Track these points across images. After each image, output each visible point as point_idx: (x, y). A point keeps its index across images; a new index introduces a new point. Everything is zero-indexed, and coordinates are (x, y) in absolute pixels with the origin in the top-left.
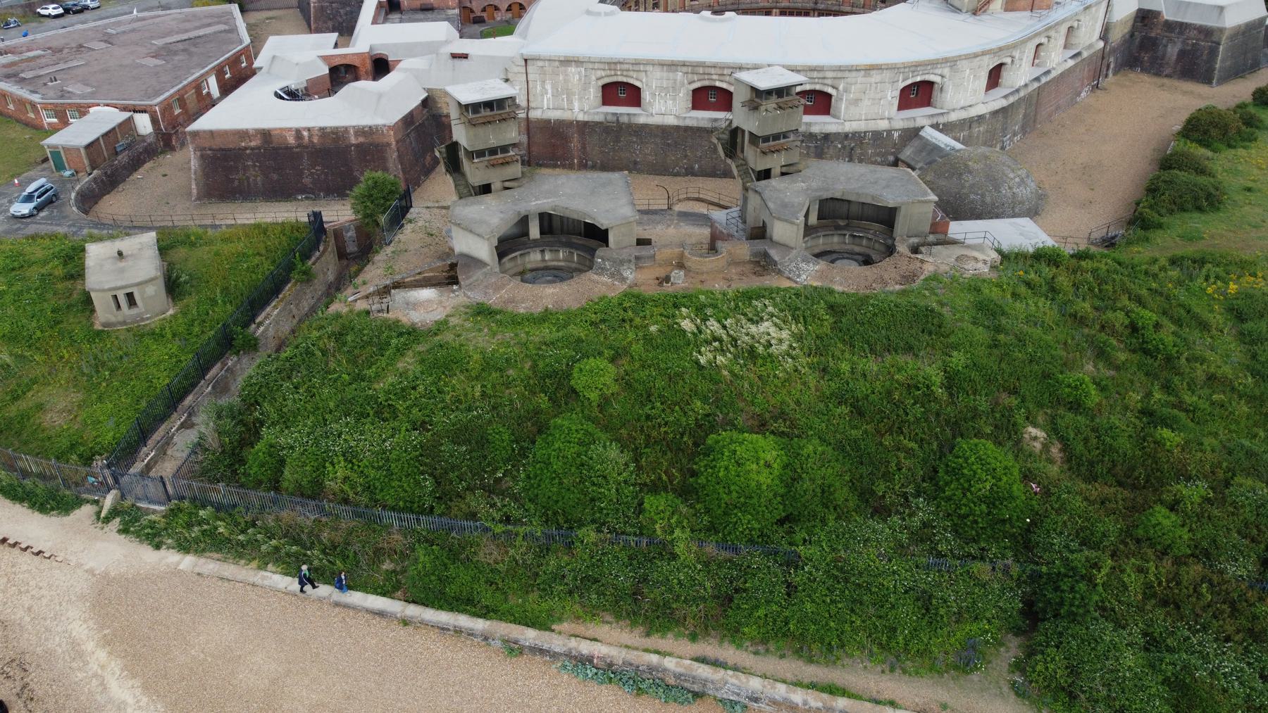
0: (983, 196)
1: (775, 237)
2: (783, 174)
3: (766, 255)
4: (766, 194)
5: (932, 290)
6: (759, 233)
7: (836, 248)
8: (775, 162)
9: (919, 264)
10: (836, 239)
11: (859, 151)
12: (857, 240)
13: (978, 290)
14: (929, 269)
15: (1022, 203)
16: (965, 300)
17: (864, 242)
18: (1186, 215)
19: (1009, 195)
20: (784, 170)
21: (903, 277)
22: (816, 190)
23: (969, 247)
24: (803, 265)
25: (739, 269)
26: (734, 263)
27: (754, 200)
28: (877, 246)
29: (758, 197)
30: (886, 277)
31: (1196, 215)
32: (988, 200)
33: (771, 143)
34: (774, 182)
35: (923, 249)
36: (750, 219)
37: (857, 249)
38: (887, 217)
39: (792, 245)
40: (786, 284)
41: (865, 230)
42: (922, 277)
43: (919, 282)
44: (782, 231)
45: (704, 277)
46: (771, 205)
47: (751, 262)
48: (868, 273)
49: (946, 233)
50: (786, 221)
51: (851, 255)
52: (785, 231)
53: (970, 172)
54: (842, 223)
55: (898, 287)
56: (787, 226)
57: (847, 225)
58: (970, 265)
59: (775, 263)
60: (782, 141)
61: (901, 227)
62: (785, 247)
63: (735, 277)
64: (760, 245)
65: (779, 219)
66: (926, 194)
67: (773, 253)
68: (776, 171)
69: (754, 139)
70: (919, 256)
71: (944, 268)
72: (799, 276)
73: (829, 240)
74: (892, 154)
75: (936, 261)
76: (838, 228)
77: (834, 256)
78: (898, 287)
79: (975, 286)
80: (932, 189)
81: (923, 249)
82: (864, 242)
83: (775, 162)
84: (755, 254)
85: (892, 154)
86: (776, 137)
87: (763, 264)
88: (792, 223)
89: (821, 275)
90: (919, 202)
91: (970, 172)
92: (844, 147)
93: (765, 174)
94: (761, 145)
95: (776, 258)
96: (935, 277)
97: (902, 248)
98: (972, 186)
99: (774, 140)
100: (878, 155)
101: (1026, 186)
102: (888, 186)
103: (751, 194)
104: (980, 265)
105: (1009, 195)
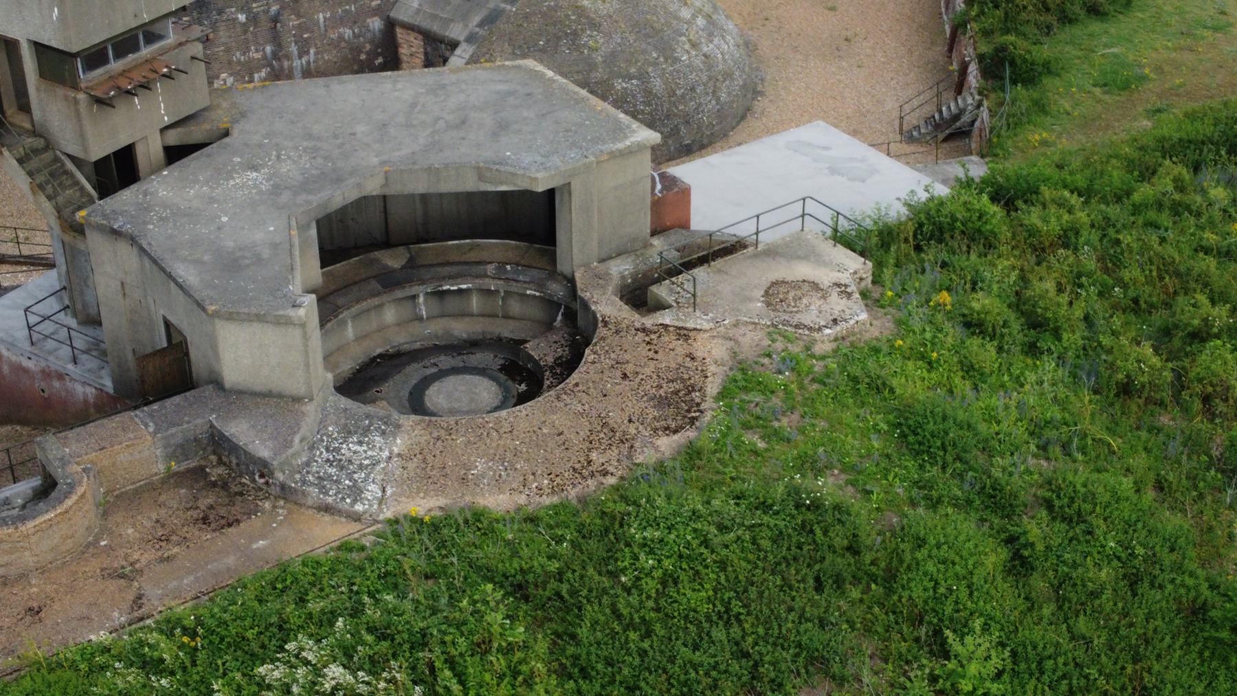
0: (643, 76)
1: (232, 374)
2: (174, 154)
3: (218, 443)
4: (155, 235)
5: (758, 423)
6: (165, 373)
7: (401, 339)
8: (142, 124)
9: (680, 347)
10: (390, 315)
11: (293, 22)
12: (452, 304)
13: (879, 387)
14: (713, 352)
15: (728, 75)
16: (862, 433)
17: (475, 303)
18: (1076, 30)
19: (698, 62)
20: (174, 138)
21: (662, 402)
22: (306, 186)
23: (772, 252)
24: (351, 448)
25: (147, 518)
26: (120, 500)
27: (111, 268)
28: (515, 307)
29: (124, 248)
30: (616, 418)
31: (1096, 26)
32: (657, 85)
33: (115, 66)
34: (162, 189)
35: (661, 291)
36: (114, 321)
37: (461, 329)
38: (530, 220)
39: (295, 386)
40: (323, 535)
41: (469, 268)
42: (712, 388)
43: (711, 410)
44: (242, 352)
45: (36, 588)
46: (187, 273)
47: (174, 479)
48: (558, 419)
49: (685, 225)
50: (260, 318)
51: (459, 353)
52: (272, 349)
53: (595, 26)
54: (393, 260)
55: (667, 444)
56: (269, 336)
57: (412, 264)
58: (812, 312)
59: (264, 469)
60: (146, 51)
61: (579, 241)
62: (275, 402)
63: (144, 557)
64: (188, 416)
65: (231, 317)
66: (619, 131)
67: (240, 430)
68: (150, 150)
69: (55, 63)
70: (666, 318)
71: (751, 340)
72: (356, 492)
73: (373, 323)
74: (376, 12)
75: (718, 324)
76: (389, 282)
77: (414, 373)
78: (667, 444)
79: (857, 374)
80: (634, 115)
81: (661, 291)
82: (475, 303)
83: (142, 124)
84: (180, 451)
85: (376, 12)
86: (125, 44)
87: (223, 480)
88: (285, 322)
89: (425, 470)
90: (613, 155)
91: (595, 26)
92: (253, 19)
93: (119, 170)
94: (87, 78)
95: (263, 451)
96: (744, 379)
97: (607, 305)
98: (612, 57)
99: (119, 55)
100: (342, 21)
101: (723, 33)
102: (502, 127)
103: (96, 243)
104: (837, 304)
105: (698, 62)
